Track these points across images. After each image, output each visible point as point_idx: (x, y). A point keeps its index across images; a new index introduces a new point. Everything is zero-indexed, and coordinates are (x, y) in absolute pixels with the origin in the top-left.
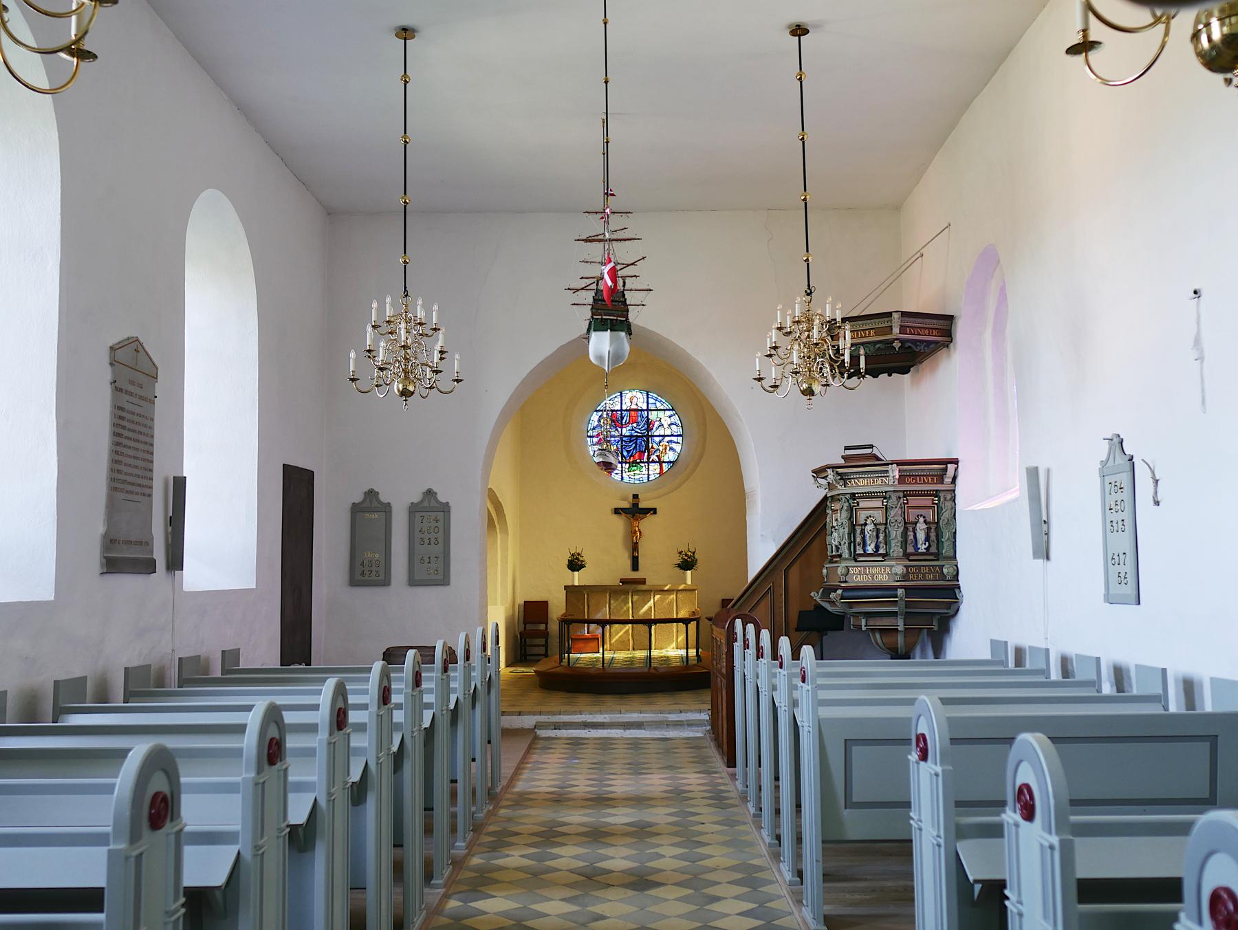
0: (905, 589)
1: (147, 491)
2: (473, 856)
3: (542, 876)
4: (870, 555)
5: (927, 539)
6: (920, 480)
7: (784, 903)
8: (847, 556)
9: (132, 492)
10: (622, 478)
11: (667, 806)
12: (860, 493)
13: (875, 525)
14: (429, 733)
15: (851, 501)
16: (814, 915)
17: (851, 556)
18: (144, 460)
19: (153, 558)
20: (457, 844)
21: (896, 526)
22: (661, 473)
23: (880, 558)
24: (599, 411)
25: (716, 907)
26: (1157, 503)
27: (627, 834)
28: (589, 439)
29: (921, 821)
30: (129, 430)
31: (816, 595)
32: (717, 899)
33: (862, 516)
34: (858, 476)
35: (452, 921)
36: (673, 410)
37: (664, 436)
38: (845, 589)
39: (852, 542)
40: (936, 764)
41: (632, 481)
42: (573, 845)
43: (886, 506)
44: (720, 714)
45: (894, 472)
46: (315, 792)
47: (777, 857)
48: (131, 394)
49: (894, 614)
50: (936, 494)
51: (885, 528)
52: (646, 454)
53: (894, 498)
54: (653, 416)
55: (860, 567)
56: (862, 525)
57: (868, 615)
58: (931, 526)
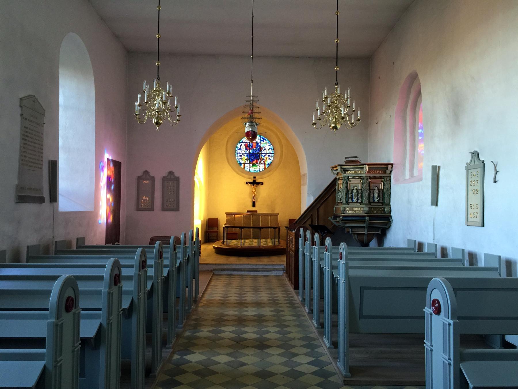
0: (369, 217)
1: (40, 166)
2: (186, 331)
3: (218, 342)
4: (355, 202)
5: (379, 196)
6: (377, 172)
7: (327, 357)
8: (345, 203)
9: (32, 166)
10: (249, 170)
11: (270, 307)
12: (351, 177)
13: (357, 190)
14: (167, 279)
15: (347, 180)
16: (344, 368)
17: (346, 203)
18: (35, 151)
19: (43, 197)
20: (179, 326)
22: (265, 168)
23: (359, 204)
24: (241, 143)
25: (295, 359)
26: (495, 182)
27: (254, 321)
28: (236, 154)
29: (432, 346)
30: (30, 138)
32: (296, 355)
33: (352, 186)
34: (350, 170)
35: (175, 367)
36: (270, 143)
37: (266, 154)
38: (344, 216)
39: (347, 197)
40: (449, 319)
41: (253, 171)
42: (231, 326)
43: (362, 182)
44: (291, 268)
45: (367, 168)
46: (101, 319)
47: (322, 334)
48: (31, 121)
49: (363, 227)
50: (383, 178)
51: (361, 192)
52: (259, 161)
53: (365, 179)
54: (262, 145)
55: (350, 207)
56: (351, 190)
57: (352, 227)
58: (380, 191)
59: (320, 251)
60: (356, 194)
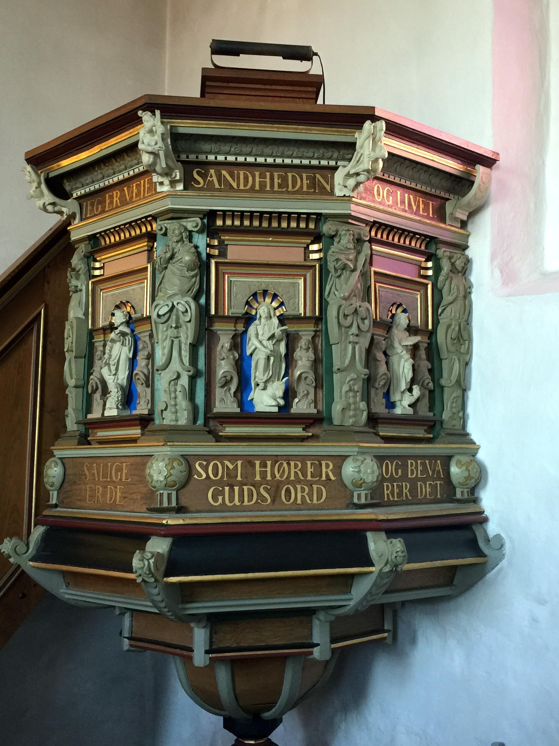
6: (403, 202)
13: (282, 320)
21: (354, 330)
23: (297, 431)
31: (21, 548)
56: (235, 319)
60: (274, 353)
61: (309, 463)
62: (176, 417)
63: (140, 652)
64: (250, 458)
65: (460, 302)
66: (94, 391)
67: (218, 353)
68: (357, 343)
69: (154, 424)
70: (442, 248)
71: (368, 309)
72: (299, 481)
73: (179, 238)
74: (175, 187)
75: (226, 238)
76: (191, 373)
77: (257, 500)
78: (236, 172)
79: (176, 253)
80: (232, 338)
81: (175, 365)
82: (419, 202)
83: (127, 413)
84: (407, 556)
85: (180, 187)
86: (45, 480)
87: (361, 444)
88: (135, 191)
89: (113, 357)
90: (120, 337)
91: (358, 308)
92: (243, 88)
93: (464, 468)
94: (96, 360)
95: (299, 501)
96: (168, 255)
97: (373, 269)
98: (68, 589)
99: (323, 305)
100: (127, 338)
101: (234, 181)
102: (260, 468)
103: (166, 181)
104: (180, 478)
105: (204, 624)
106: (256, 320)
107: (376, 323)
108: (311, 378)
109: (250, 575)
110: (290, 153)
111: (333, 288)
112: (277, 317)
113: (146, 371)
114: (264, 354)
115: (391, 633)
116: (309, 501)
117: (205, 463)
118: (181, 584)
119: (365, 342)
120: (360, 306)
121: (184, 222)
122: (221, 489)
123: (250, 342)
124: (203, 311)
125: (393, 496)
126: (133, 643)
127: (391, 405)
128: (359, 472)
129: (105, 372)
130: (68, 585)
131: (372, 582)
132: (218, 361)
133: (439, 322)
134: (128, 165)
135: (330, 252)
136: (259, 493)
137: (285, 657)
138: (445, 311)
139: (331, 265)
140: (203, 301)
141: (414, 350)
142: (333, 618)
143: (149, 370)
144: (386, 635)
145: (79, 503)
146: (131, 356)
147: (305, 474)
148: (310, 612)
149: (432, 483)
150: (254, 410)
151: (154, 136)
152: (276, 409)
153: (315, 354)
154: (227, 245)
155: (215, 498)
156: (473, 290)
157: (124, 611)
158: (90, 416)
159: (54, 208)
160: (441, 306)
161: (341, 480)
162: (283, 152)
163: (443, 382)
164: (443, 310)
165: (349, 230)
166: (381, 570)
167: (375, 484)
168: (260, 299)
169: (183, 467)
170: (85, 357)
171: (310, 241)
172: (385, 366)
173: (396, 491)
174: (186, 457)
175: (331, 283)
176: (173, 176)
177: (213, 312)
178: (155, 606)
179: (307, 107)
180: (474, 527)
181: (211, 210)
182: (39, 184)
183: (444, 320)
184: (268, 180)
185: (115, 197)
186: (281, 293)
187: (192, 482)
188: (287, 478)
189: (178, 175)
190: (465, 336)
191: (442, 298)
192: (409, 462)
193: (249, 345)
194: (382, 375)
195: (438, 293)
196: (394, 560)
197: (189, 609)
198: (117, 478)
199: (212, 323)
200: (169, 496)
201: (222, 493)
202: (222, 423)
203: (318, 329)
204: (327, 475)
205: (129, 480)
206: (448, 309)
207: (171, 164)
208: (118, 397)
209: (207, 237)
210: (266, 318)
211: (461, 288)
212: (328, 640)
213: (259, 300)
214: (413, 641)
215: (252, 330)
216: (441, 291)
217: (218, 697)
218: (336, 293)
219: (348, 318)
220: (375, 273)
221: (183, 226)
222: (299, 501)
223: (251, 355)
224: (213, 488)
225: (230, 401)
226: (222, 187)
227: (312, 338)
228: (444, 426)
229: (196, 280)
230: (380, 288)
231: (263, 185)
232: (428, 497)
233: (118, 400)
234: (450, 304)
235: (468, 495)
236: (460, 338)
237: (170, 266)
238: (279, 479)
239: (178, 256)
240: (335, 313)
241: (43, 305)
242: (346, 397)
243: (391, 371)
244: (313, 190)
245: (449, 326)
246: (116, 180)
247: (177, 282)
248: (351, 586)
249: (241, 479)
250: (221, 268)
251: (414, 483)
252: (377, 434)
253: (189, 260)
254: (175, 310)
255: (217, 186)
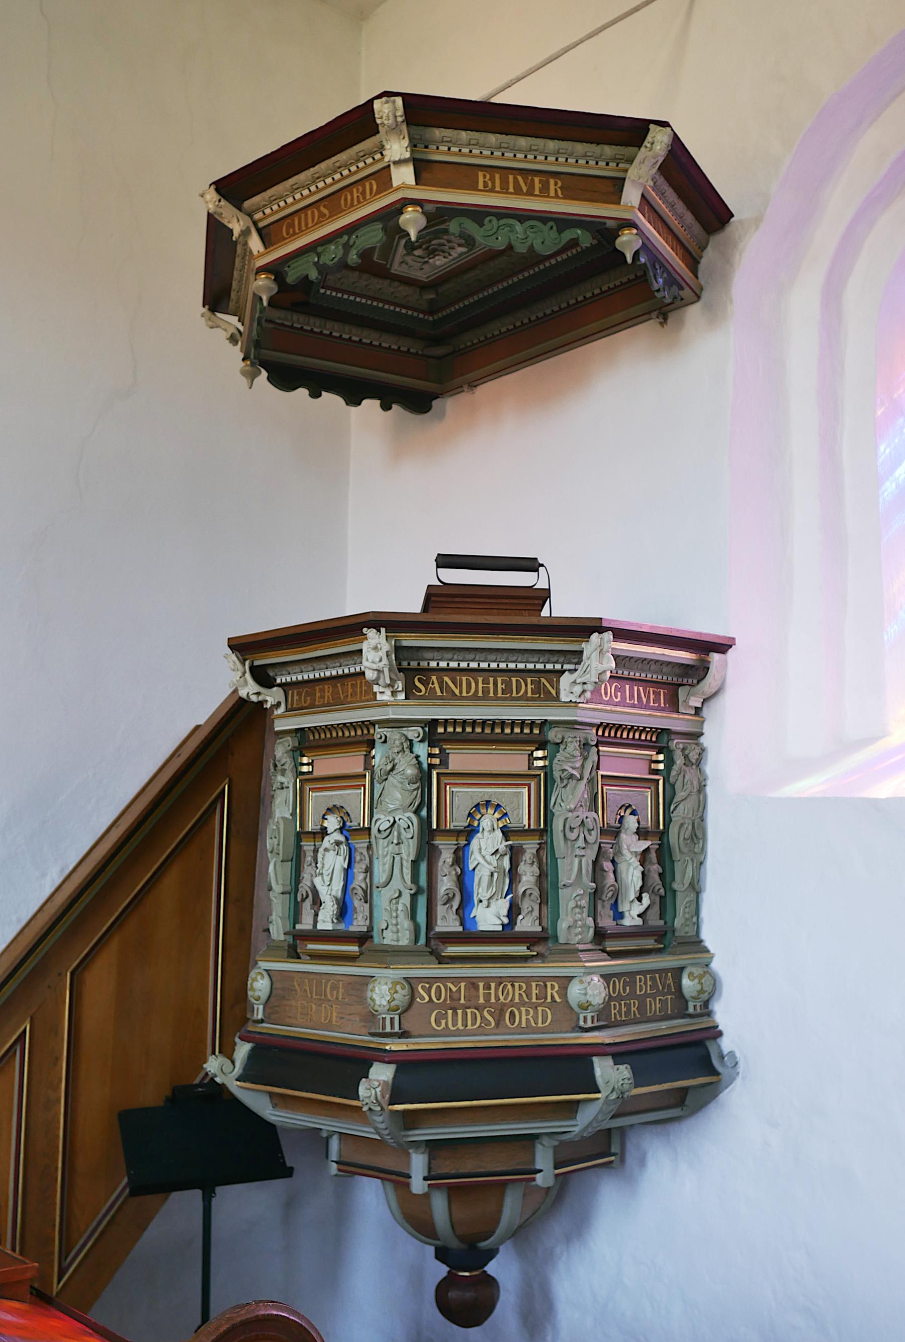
6: (632, 697)
13: (507, 833)
21: (581, 843)
23: (521, 950)
56: (457, 833)
59: (262, 249)
60: (499, 868)
61: (534, 984)
62: (398, 936)
63: (350, 1176)
64: (474, 980)
65: (694, 797)
66: (303, 900)
67: (439, 869)
68: (583, 856)
69: (372, 941)
70: (673, 740)
71: (595, 819)
72: (524, 1004)
73: (400, 748)
74: (396, 696)
75: (448, 746)
76: (412, 892)
77: (481, 1023)
78: (458, 678)
79: (397, 764)
80: (454, 853)
81: (396, 883)
82: (649, 692)
83: (342, 927)
84: (633, 1084)
85: (402, 696)
86: (250, 993)
87: (587, 964)
88: (350, 690)
89: (326, 867)
90: (334, 846)
91: (585, 819)
92: (467, 602)
93: (697, 981)
94: (305, 866)
95: (524, 1025)
96: (389, 767)
97: (600, 773)
98: (275, 1111)
99: (549, 816)
100: (341, 846)
101: (456, 687)
102: (484, 990)
103: (388, 692)
104: (403, 1002)
105: (423, 1150)
106: (478, 832)
107: (603, 832)
108: (536, 894)
109: (475, 1103)
110: (514, 658)
111: (559, 800)
112: (501, 828)
113: (364, 886)
114: (488, 870)
115: (618, 1156)
116: (534, 1025)
117: (427, 986)
118: (405, 1112)
119: (591, 854)
120: (587, 817)
121: (404, 731)
122: (444, 1012)
123: (473, 856)
124: (425, 823)
125: (621, 1016)
126: (342, 1167)
127: (619, 916)
128: (586, 994)
129: (318, 881)
130: (275, 1106)
131: (598, 1109)
132: (439, 877)
133: (671, 820)
134: (344, 664)
135: (556, 761)
136: (482, 1017)
137: (504, 1184)
138: (678, 809)
139: (557, 774)
140: (424, 813)
141: (644, 857)
142: (556, 1143)
143: (367, 884)
144: (612, 1158)
145: (288, 1020)
146: (346, 866)
147: (529, 996)
148: (532, 1139)
149: (662, 998)
150: (476, 928)
151: (378, 652)
152: (500, 928)
153: (539, 869)
154: (449, 753)
155: (438, 1023)
156: (709, 783)
157: (331, 1133)
158: (298, 927)
159: (258, 697)
160: (674, 802)
161: (567, 1002)
162: (507, 658)
163: (675, 886)
164: (676, 807)
165: (575, 737)
166: (607, 1097)
167: (602, 1006)
168: (483, 811)
169: (406, 991)
170: (292, 861)
171: (534, 748)
172: (612, 876)
173: (624, 1009)
174: (409, 979)
175: (557, 792)
176: (396, 687)
177: (435, 827)
178: (378, 1133)
179: (533, 620)
180: (708, 1043)
181: (433, 720)
182: (244, 673)
183: (676, 818)
184: (491, 686)
185: (326, 692)
186: (505, 804)
187: (415, 1006)
188: (511, 1000)
189: (400, 685)
190: (700, 835)
191: (674, 794)
192: (638, 977)
193: (472, 859)
194: (610, 886)
195: (671, 789)
196: (620, 1088)
197: (409, 1136)
198: (332, 995)
199: (433, 837)
200: (392, 1019)
201: (445, 1016)
202: (444, 943)
203: (543, 841)
204: (552, 997)
205: (346, 1000)
206: (681, 806)
207: (393, 677)
208: (333, 911)
209: (429, 746)
210: (489, 831)
211: (695, 783)
212: (551, 1165)
213: (482, 811)
214: (642, 1162)
215: (475, 843)
216: (673, 786)
217: (433, 1225)
218: (562, 804)
219: (575, 830)
220: (602, 776)
221: (404, 735)
222: (524, 1025)
223: (474, 869)
224: (436, 1012)
225: (452, 919)
226: (445, 694)
227: (537, 851)
228: (676, 934)
229: (417, 794)
230: (607, 791)
231: (486, 691)
232: (658, 1013)
233: (333, 915)
234: (683, 800)
235: (701, 1009)
236: (694, 837)
237: (390, 778)
238: (504, 1001)
239: (399, 768)
240: (561, 827)
241: (227, 780)
242: (572, 913)
243: (619, 882)
244: (537, 696)
245: (682, 825)
246: (328, 674)
247: (399, 796)
248: (577, 1112)
249: (464, 1002)
250: (442, 778)
251: (642, 999)
252: (603, 951)
253: (411, 775)
254: (396, 825)
255: (439, 693)
